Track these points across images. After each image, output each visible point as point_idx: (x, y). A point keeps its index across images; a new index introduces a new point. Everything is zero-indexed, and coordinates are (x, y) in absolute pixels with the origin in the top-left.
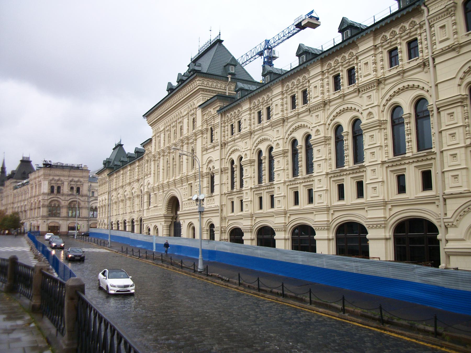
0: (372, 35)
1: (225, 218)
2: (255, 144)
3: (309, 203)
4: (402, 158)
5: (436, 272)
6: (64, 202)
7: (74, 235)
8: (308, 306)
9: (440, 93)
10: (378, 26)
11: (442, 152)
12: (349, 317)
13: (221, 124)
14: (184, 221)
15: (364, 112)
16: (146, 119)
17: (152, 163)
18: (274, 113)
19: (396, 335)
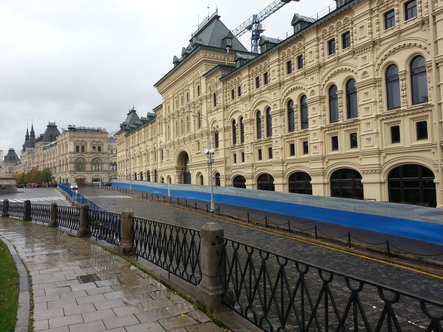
1: (229, 168)
2: (254, 106)
3: (304, 154)
4: (397, 111)
5: (438, 212)
6: (104, 159)
7: (99, 186)
8: (314, 240)
9: (439, 50)
11: (440, 104)
13: (223, 90)
14: (193, 171)
15: (358, 72)
16: (156, 89)
17: (164, 125)
18: (272, 78)
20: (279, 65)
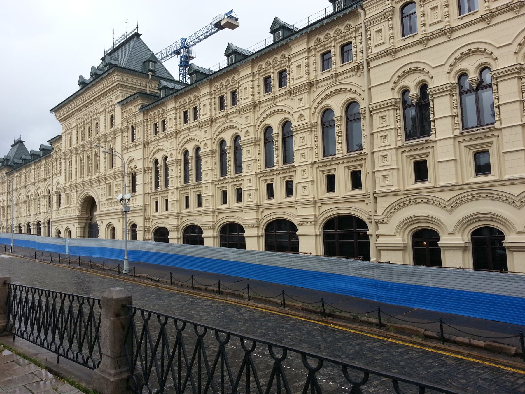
0: (306, 37)
2: (181, 144)
8: (246, 301)
10: (313, 28)
11: (373, 153)
12: (290, 311)
13: (144, 122)
14: (102, 222)
17: (63, 161)
19: (341, 328)
20: (211, 99)
